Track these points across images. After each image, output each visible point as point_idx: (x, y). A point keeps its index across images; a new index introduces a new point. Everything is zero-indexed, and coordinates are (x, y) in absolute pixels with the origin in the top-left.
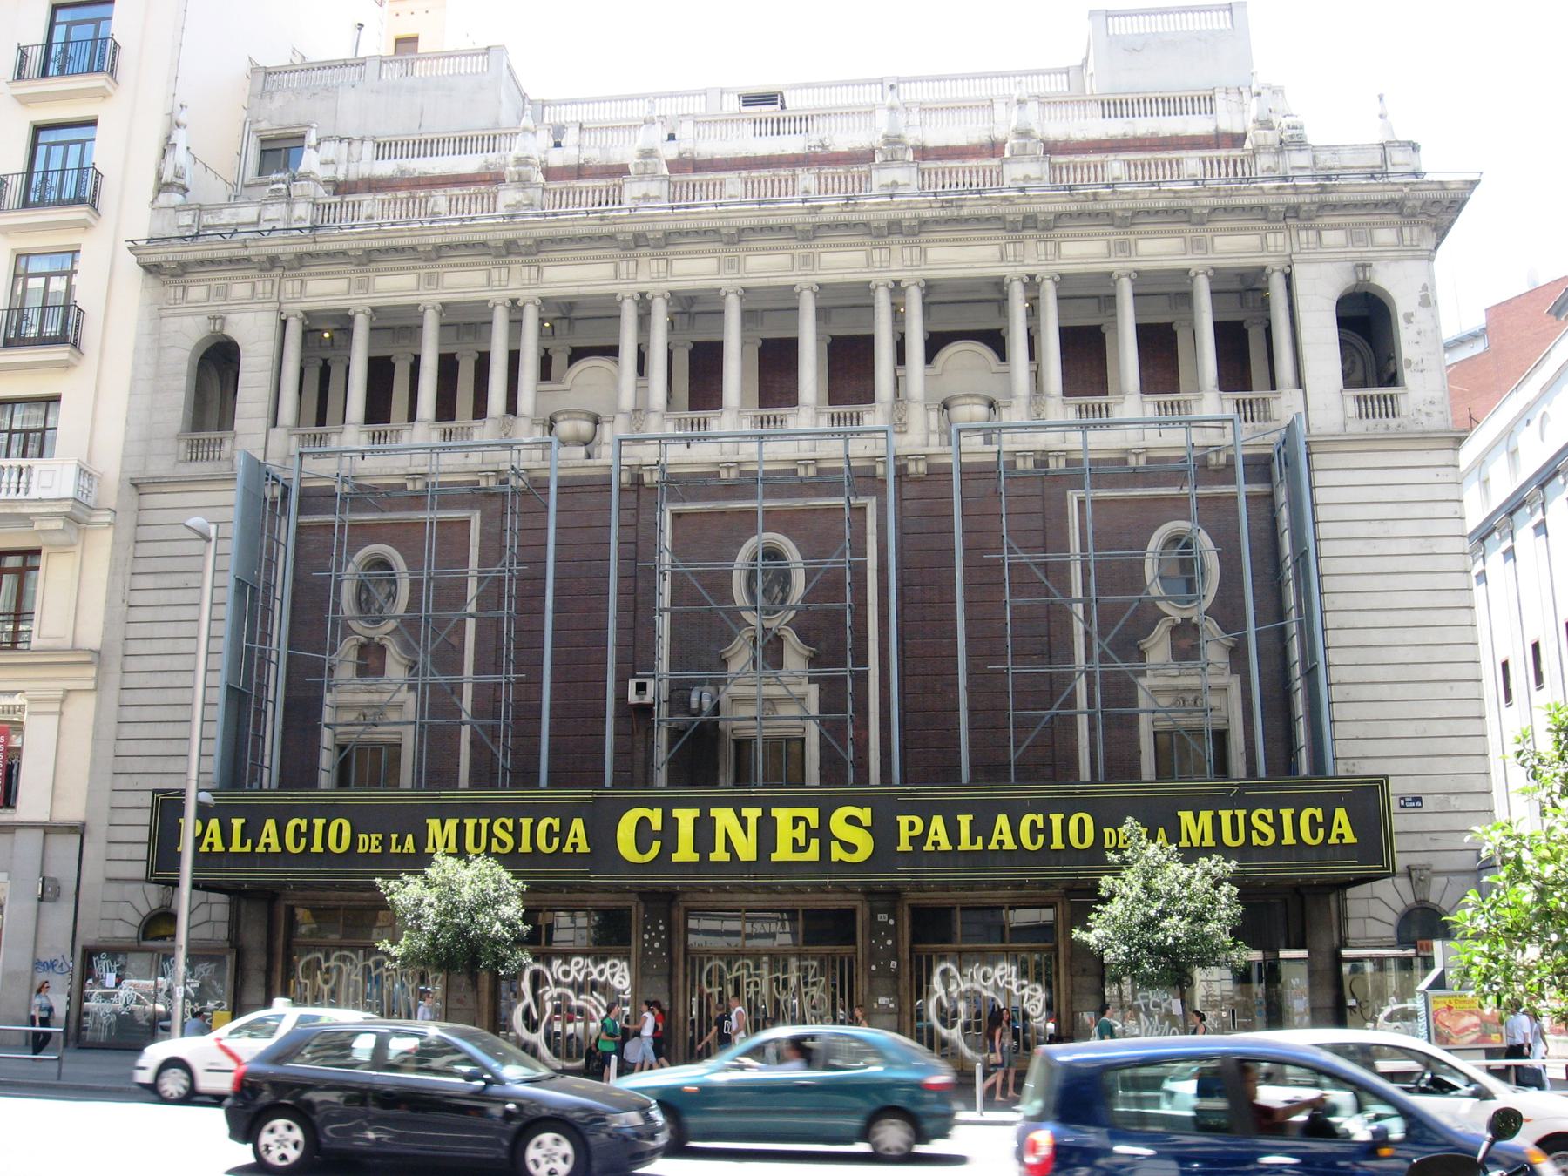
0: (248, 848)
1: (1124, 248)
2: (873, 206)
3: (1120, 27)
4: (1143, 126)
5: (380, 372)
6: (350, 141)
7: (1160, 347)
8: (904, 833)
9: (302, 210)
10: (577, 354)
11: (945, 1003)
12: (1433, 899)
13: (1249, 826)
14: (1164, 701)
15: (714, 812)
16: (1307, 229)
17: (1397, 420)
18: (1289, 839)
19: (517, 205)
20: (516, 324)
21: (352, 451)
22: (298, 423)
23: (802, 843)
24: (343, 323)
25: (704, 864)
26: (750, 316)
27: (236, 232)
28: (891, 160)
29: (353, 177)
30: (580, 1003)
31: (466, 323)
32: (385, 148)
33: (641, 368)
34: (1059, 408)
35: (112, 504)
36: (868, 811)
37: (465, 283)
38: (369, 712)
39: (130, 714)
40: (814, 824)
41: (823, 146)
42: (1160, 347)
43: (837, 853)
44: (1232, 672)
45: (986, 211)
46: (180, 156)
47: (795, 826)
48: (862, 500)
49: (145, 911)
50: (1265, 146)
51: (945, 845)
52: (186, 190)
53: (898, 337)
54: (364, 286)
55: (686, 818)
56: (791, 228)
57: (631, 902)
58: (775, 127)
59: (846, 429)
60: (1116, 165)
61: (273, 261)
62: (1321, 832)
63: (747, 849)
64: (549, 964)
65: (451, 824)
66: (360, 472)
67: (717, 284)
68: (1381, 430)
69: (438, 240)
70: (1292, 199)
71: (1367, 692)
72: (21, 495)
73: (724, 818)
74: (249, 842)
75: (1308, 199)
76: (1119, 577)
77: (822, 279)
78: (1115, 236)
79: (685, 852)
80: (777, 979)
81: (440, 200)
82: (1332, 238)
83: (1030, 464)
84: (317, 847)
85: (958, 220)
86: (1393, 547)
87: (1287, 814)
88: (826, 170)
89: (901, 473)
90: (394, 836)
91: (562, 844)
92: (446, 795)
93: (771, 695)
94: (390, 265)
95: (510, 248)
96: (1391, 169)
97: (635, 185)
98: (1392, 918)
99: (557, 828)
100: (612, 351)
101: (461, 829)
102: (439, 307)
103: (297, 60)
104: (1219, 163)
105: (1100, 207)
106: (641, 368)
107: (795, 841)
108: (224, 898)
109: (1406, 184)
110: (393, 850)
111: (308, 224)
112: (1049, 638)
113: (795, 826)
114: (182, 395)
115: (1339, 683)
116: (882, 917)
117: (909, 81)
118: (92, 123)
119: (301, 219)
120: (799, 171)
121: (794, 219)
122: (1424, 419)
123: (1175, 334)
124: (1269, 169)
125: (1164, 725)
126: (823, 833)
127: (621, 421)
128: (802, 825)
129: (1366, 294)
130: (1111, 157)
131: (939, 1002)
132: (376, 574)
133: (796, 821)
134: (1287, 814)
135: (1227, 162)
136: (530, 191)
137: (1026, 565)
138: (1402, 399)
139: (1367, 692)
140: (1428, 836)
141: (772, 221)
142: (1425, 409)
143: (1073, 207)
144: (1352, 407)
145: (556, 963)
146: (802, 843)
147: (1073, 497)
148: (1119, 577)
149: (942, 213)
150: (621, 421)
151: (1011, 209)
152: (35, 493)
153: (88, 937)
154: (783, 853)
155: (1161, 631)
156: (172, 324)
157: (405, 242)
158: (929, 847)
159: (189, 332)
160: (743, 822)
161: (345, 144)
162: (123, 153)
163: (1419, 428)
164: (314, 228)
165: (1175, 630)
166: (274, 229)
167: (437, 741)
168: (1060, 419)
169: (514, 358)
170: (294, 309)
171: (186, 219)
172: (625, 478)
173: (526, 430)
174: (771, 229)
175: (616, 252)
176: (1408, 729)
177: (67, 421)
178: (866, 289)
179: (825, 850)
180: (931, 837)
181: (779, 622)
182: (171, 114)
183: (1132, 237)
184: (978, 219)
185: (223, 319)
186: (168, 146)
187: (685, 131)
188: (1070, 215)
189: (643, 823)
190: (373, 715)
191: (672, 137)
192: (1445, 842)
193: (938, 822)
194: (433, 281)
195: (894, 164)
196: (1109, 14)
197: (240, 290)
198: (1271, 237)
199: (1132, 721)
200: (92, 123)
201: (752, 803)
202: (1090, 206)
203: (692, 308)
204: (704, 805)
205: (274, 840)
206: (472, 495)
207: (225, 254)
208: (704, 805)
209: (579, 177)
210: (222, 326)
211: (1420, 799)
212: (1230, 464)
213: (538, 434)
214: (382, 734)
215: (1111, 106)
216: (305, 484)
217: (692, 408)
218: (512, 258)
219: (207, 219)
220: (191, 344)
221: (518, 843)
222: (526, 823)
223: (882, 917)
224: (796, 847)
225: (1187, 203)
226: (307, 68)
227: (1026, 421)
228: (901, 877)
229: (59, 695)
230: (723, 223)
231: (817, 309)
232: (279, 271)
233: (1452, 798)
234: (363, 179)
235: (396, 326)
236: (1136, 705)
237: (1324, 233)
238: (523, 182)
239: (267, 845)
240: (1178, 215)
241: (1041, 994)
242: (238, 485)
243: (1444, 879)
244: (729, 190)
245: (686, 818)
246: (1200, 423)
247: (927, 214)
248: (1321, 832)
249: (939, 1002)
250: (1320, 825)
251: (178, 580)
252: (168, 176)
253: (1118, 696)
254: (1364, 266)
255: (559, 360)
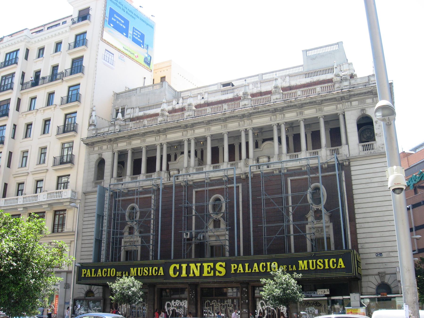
0: (250, 271)
1: (321, 110)
2: (238, 111)
3: (310, 53)
4: (315, 79)
5: (231, 148)
6: (134, 108)
7: (315, 137)
8: (233, 269)
9: (117, 127)
10: (264, 141)
11: (262, 311)
12: (386, 281)
13: (317, 264)
14: (313, 231)
15: (190, 265)
16: (348, 102)
17: (374, 150)
18: (327, 267)
19: (162, 121)
20: (247, 135)
21: (129, 182)
22: (307, 150)
23: (209, 271)
24: (205, 139)
25: (188, 277)
26: (306, 126)
27: (104, 134)
28: (245, 99)
29: (134, 117)
30: (178, 311)
31: (235, 136)
32: (141, 109)
33: (189, 156)
34: (285, 157)
35: (80, 198)
36: (224, 263)
37: (150, 141)
38: (131, 243)
39: (84, 246)
40: (212, 267)
41: (237, 95)
42: (315, 137)
43: (217, 274)
44: (330, 222)
45: (264, 109)
46: (94, 118)
47: (208, 268)
48: (238, 185)
49: (86, 290)
50: (337, 81)
51: (242, 271)
52: (95, 125)
53: (255, 141)
54: (130, 143)
55: (184, 266)
56: (220, 119)
57: (187, 286)
58: (232, 91)
59: (295, 158)
60: (299, 92)
61: (110, 140)
62: (335, 265)
63: (197, 274)
64: (171, 302)
65: (135, 269)
66: (129, 187)
67: (205, 135)
68: (369, 153)
69: (143, 131)
70: (341, 95)
71: (366, 225)
72: (60, 198)
73: (192, 266)
74: (250, 269)
75: (346, 94)
76: (201, 209)
77: (147, 145)
78: (318, 107)
79: (184, 274)
80: (222, 305)
81: (146, 122)
82: (354, 103)
83: (277, 172)
84: (109, 275)
85: (258, 112)
86: (373, 185)
87: (326, 261)
88: (230, 103)
89: (322, 168)
90: (290, 266)
91: (337, 266)
92: (117, 263)
93: (217, 235)
94: (215, 124)
95: (159, 132)
96: (371, 83)
97: (187, 113)
98: (374, 287)
99: (335, 261)
100: (272, 139)
101: (137, 270)
102: (227, 133)
103: (127, 90)
104: (325, 87)
105: (292, 104)
106: (189, 156)
107: (208, 271)
108: (101, 287)
109: (372, 87)
110: (290, 270)
111: (118, 131)
112: (280, 217)
113: (208, 268)
114: (93, 172)
115: (359, 223)
116: (244, 289)
117: (265, 74)
118: (76, 112)
119: (117, 129)
120: (223, 104)
121: (220, 117)
122: (381, 149)
123: (235, 146)
124: (338, 87)
125: (313, 237)
126: (214, 269)
127: (184, 170)
128: (210, 267)
129: (363, 118)
130: (298, 90)
131: (260, 310)
132: (217, 202)
133: (208, 266)
134: (326, 261)
135: (328, 87)
136: (164, 117)
137: (269, 199)
138: (375, 145)
139: (366, 225)
140: (384, 264)
141: (215, 118)
142: (381, 146)
143: (286, 105)
144: (361, 148)
145: (173, 301)
146: (209, 271)
147: (289, 179)
148: (201, 209)
149: (254, 111)
150: (184, 170)
151: (271, 108)
152: (63, 197)
153: (76, 297)
154: (205, 274)
155: (211, 220)
156: (92, 156)
157: (151, 130)
158: (238, 272)
159: (95, 158)
160: (197, 267)
161: (132, 109)
162: (82, 120)
163: (380, 152)
164: (120, 131)
165: (214, 221)
166: (111, 133)
167: (145, 250)
168: (286, 160)
169: (247, 144)
170: (116, 150)
171: (94, 132)
172: (252, 175)
173: (252, 162)
174: (215, 120)
175: (182, 130)
176: (378, 235)
177: (71, 180)
178: (239, 132)
179: (215, 273)
180: (239, 269)
181: (321, 207)
182: (92, 108)
183: (303, 110)
184: (263, 111)
185: (101, 154)
186: (91, 116)
187: (206, 96)
188: (286, 107)
189: (175, 267)
190: (133, 243)
191: (203, 98)
192: (389, 265)
193: (240, 265)
194: (144, 141)
195: (245, 100)
196: (307, 51)
197: (105, 147)
198: (339, 106)
199: (304, 238)
200: (76, 112)
201: (198, 262)
202: (290, 104)
203: (292, 126)
204: (188, 263)
205: (100, 274)
206: (239, 179)
207: (100, 140)
208: (188, 263)
209: (175, 112)
210: (101, 156)
211: (382, 254)
212: (317, 168)
213: (255, 163)
214: (134, 248)
215: (307, 75)
216: (176, 183)
217: (295, 152)
218: (244, 118)
219: (98, 132)
220: (95, 161)
221: (149, 273)
222: (151, 268)
223: (244, 289)
224: (208, 273)
225: (314, 100)
226: (130, 91)
227: (277, 161)
228: (232, 279)
229: (69, 242)
230: (204, 120)
231: (305, 125)
232: (112, 142)
233: (391, 253)
234: (136, 117)
235: (217, 139)
236: (306, 232)
237: (352, 102)
238: (163, 115)
239: (255, 270)
240: (312, 103)
241: (285, 309)
242: (97, 193)
243: (389, 276)
244: (208, 111)
245: (184, 266)
246: (139, 181)
247: (251, 112)
248: (335, 265)
249: (260, 310)
250: (335, 263)
251: (379, 184)
252: (91, 123)
253: (300, 230)
254: (363, 110)
255: (260, 143)
